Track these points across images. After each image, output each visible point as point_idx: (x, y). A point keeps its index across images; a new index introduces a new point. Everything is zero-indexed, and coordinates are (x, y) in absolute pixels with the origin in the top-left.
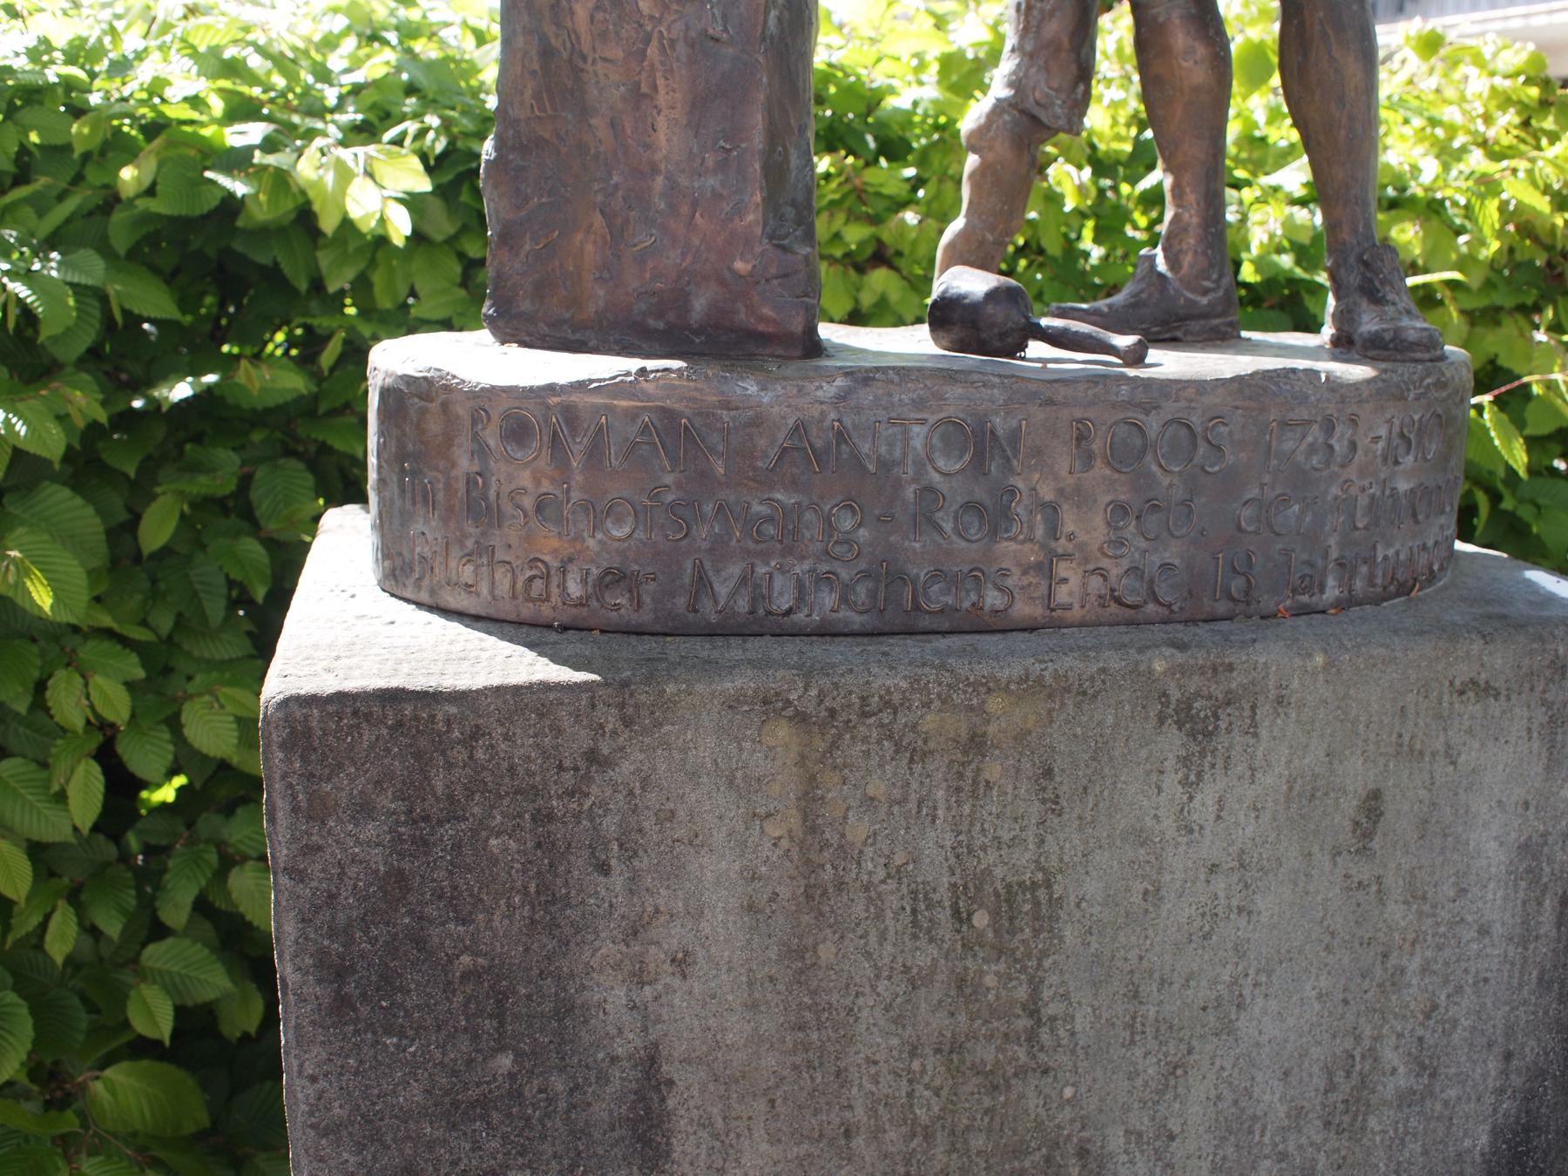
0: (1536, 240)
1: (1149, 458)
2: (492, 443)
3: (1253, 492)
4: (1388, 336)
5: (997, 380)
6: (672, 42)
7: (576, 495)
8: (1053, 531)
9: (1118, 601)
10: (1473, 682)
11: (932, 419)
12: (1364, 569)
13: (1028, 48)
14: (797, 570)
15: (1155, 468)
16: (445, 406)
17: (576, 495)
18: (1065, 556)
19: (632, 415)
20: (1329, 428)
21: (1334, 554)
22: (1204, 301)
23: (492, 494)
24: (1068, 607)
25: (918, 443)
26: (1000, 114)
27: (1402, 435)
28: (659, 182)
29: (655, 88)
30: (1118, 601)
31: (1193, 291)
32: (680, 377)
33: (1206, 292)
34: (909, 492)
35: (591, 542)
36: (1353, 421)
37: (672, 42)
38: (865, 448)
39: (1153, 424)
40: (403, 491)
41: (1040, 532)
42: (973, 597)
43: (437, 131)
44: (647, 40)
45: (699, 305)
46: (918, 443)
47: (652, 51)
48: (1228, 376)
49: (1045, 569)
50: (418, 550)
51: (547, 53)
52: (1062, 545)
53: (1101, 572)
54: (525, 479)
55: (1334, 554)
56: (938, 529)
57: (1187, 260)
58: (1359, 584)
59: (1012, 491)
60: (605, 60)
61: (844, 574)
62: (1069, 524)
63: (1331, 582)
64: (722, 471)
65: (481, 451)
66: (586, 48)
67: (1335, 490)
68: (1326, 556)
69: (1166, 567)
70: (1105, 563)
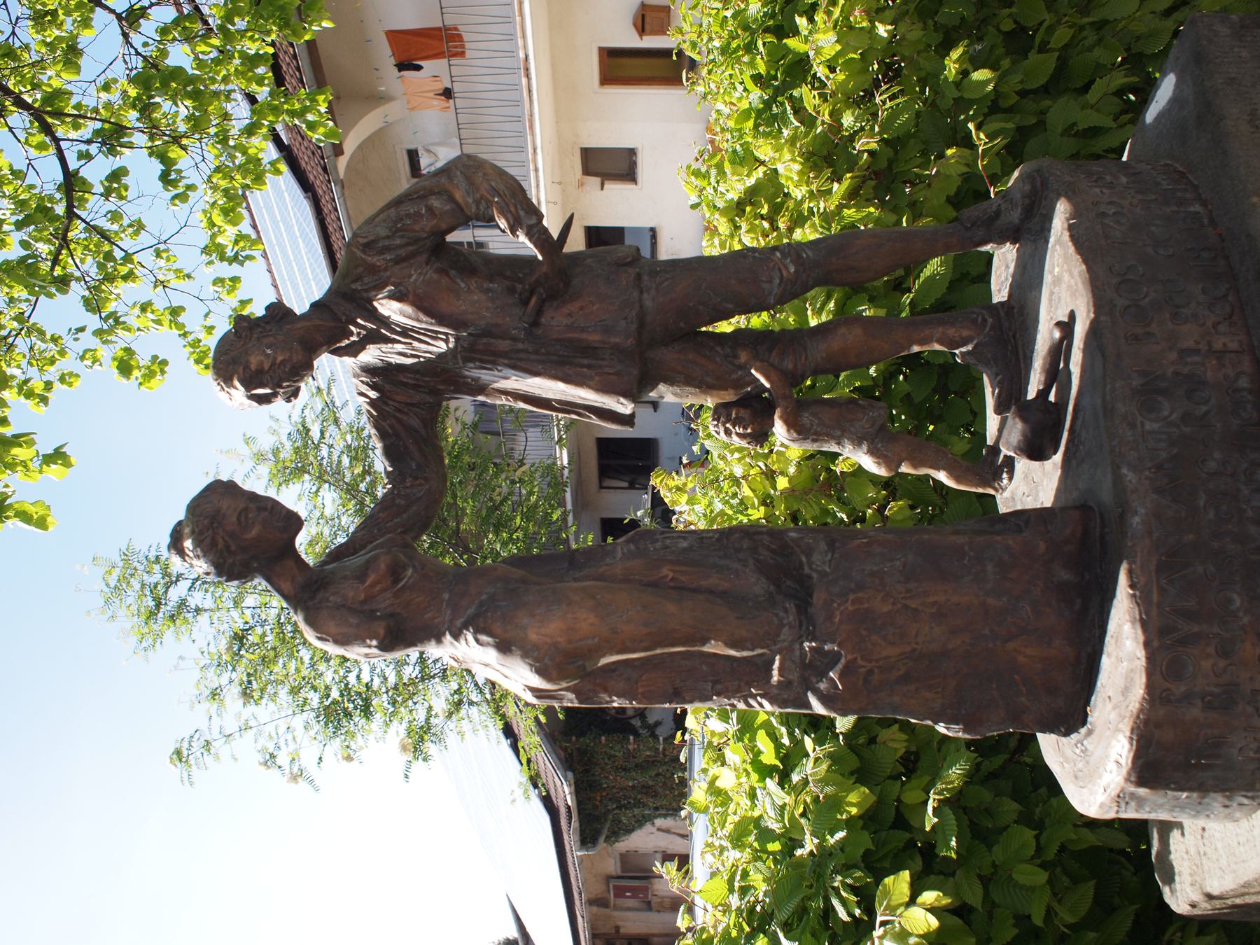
0: (860, 187)
1: (1141, 303)
2: (1183, 689)
3: (1150, 250)
4: (1027, 201)
5: (1109, 386)
6: (908, 591)
7: (1216, 630)
8: (1196, 352)
9: (1231, 316)
10: (1249, 122)
11: (1140, 419)
12: (1179, 194)
13: (839, 433)
14: (1246, 492)
15: (1146, 300)
16: (1158, 725)
17: (1216, 630)
18: (1209, 344)
19: (1162, 591)
20: (1104, 214)
21: (1175, 209)
22: (990, 320)
23: (1216, 690)
24: (1240, 341)
25: (1156, 426)
26: (878, 450)
27: (1096, 181)
28: (990, 601)
29: (935, 603)
30: (1231, 316)
31: (985, 326)
32: (1135, 562)
33: (985, 320)
34: (1187, 430)
35: (1246, 620)
36: (1096, 204)
37: (908, 591)
38: (1164, 454)
39: (1121, 302)
40: (1208, 767)
41: (1197, 359)
42: (1245, 393)
43: (845, 877)
44: (906, 607)
45: (1064, 575)
46: (1156, 426)
47: (913, 604)
48: (1084, 267)
49: (1220, 355)
50: (1251, 754)
51: (906, 678)
52: (1203, 346)
53: (1215, 326)
54: (1206, 664)
55: (1175, 209)
56: (1207, 413)
57: (965, 333)
58: (1188, 195)
59: (1176, 374)
60: (916, 635)
61: (1245, 465)
62: (1190, 343)
63: (1192, 209)
64: (1191, 536)
65: (1187, 697)
66: (909, 649)
67: (1138, 210)
68: (1177, 212)
69: (1204, 291)
70: (1209, 324)
